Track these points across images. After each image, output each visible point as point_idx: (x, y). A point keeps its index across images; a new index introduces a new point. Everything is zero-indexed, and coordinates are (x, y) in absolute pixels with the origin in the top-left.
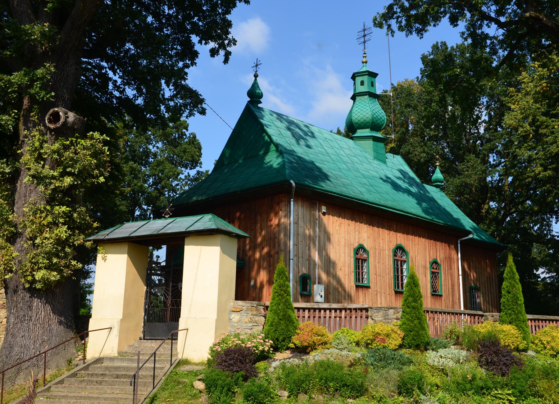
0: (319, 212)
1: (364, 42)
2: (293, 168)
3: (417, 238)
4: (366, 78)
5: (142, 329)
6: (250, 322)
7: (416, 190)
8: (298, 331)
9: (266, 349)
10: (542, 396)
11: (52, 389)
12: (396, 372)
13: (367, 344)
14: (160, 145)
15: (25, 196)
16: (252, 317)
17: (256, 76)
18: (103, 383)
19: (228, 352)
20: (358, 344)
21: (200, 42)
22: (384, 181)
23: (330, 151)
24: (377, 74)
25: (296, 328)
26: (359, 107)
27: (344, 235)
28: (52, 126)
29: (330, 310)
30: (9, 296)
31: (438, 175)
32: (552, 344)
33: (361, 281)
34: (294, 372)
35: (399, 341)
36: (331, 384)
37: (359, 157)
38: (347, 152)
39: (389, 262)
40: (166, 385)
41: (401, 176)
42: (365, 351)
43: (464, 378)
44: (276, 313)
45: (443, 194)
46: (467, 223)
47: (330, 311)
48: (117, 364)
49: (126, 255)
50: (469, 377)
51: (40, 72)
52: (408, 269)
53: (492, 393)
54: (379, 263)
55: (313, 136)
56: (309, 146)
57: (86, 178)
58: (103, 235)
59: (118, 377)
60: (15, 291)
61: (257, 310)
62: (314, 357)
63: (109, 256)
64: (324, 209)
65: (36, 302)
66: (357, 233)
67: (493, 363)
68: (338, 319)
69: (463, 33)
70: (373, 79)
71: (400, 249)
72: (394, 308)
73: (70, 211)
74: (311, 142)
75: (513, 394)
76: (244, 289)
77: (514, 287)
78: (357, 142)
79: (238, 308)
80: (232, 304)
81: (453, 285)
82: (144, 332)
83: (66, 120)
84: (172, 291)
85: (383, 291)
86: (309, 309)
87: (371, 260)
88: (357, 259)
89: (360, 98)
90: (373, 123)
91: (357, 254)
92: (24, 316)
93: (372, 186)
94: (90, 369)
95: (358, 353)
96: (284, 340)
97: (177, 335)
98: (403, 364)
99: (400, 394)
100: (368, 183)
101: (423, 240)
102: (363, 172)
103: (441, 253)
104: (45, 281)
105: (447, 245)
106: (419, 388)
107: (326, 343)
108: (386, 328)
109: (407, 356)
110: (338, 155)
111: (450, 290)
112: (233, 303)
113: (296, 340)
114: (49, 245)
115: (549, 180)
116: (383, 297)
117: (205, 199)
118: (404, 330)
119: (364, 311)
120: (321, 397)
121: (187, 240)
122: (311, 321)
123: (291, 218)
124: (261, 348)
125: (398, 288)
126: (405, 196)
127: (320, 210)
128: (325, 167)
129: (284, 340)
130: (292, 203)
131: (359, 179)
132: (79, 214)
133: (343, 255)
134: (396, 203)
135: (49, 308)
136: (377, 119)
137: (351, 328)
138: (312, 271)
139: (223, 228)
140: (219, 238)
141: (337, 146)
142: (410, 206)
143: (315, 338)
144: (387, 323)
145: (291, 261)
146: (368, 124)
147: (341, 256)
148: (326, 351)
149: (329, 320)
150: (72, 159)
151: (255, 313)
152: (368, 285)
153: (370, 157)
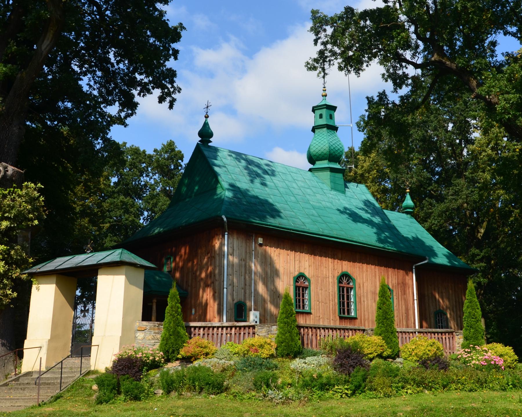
0: (255, 243)
3: (365, 266)
4: (324, 112)
5: (70, 349)
6: (153, 339)
7: (380, 220)
10: (375, 390)
13: (244, 355)
14: (157, 176)
16: (154, 335)
17: (207, 117)
18: (26, 389)
21: (139, 94)
22: (342, 212)
26: (317, 140)
27: (288, 263)
31: (408, 201)
33: (346, 313)
37: (313, 189)
38: (300, 184)
39: (333, 289)
45: (414, 220)
47: (222, 329)
49: (54, 286)
53: (334, 389)
54: (321, 290)
56: (264, 184)
57: (22, 221)
58: (35, 269)
61: (159, 329)
63: (42, 286)
64: (260, 241)
66: (297, 262)
68: (229, 335)
69: (383, 75)
70: (332, 112)
73: (8, 250)
78: (316, 174)
79: (143, 328)
80: (137, 324)
81: (407, 310)
82: (72, 351)
83: (5, 173)
86: (204, 328)
87: (312, 287)
88: (340, 287)
89: (319, 130)
90: (330, 154)
91: (297, 282)
93: (319, 216)
94: (20, 380)
96: (173, 352)
100: (316, 214)
102: (314, 204)
110: (288, 188)
111: (404, 315)
112: (139, 323)
119: (251, 328)
120: (189, 394)
125: (344, 313)
129: (173, 352)
130: (226, 236)
131: (306, 210)
132: (16, 251)
134: (343, 233)
136: (334, 150)
137: (235, 342)
140: (124, 269)
141: (290, 179)
142: (365, 235)
146: (326, 156)
149: (221, 337)
150: (9, 206)
151: (157, 331)
152: (309, 311)
153: (327, 187)
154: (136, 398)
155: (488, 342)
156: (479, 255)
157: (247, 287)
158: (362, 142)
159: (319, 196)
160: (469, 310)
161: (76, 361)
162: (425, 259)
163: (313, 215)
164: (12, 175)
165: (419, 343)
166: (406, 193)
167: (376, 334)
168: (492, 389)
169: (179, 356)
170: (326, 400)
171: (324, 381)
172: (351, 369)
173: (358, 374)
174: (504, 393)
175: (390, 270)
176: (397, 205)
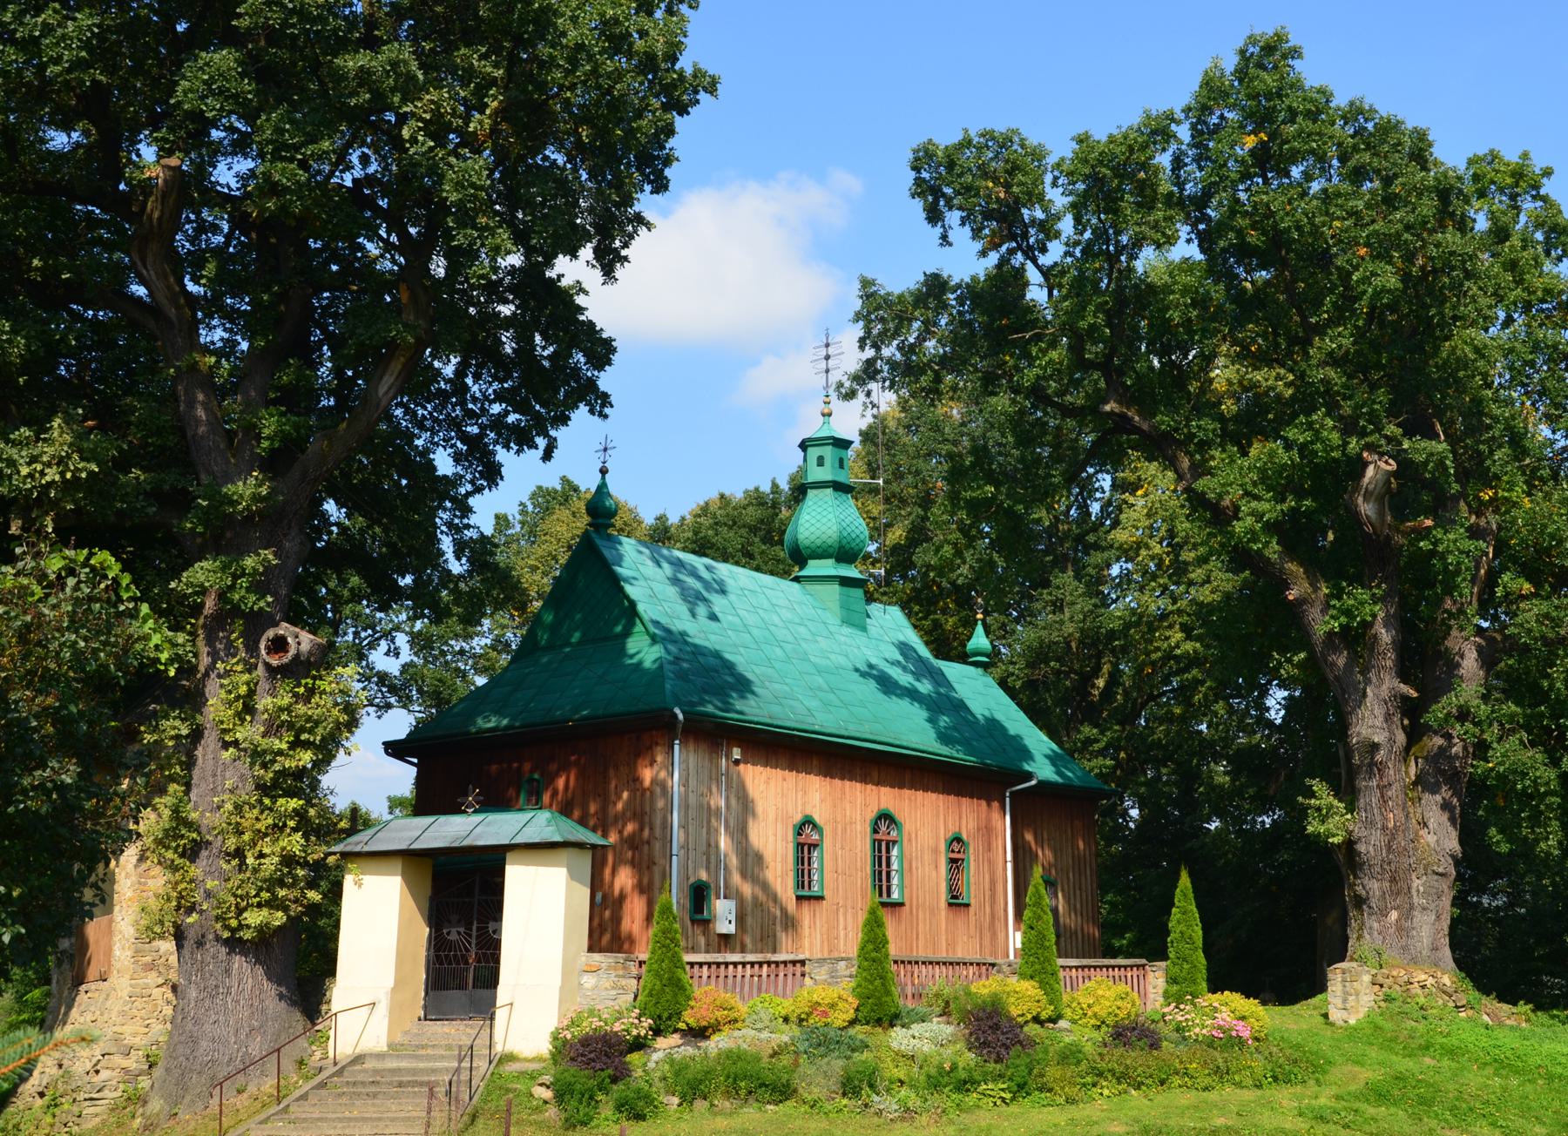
2: (682, 676)
4: (828, 452)
8: (692, 1003)
9: (643, 1033)
10: (1050, 1090)
11: (291, 1109)
12: (841, 1063)
13: (801, 1020)
15: (215, 775)
17: (604, 471)
19: (586, 1041)
20: (786, 1020)
22: (864, 675)
23: (751, 619)
25: (689, 998)
27: (778, 797)
28: (275, 662)
29: (744, 964)
30: (186, 952)
32: (1096, 1009)
34: (687, 1067)
35: (851, 1015)
36: (743, 1084)
40: (489, 1094)
41: (901, 658)
42: (796, 1031)
43: (940, 1067)
44: (658, 975)
46: (1038, 742)
48: (391, 1064)
50: (947, 1066)
51: (249, 562)
52: (901, 857)
55: (723, 592)
56: (713, 617)
59: (400, 1085)
60: (200, 944)
61: (625, 968)
62: (717, 1043)
64: (737, 753)
65: (238, 961)
67: (985, 1044)
70: (842, 453)
71: (885, 818)
72: (847, 959)
74: (718, 603)
75: (1008, 1089)
76: (605, 932)
77: (1039, 918)
81: (993, 883)
82: (425, 1007)
84: (478, 937)
85: (849, 903)
86: (709, 964)
89: (815, 492)
90: (841, 547)
92: (217, 986)
95: (784, 1035)
96: (669, 1018)
97: (493, 1014)
98: (853, 1050)
99: (844, 1094)
101: (932, 797)
104: (262, 929)
105: (984, 803)
106: (871, 1086)
107: (736, 1021)
108: (831, 994)
109: (860, 1037)
111: (988, 893)
113: (689, 1018)
114: (270, 865)
115: (1193, 661)
116: (849, 916)
117: (507, 728)
118: (859, 996)
120: (727, 1104)
121: (509, 856)
122: (712, 987)
123: (674, 772)
124: (635, 1032)
126: (904, 706)
127: (728, 756)
128: (743, 660)
129: (669, 1018)
130: (677, 748)
133: (771, 839)
135: (260, 971)
139: (572, 838)
140: (564, 854)
141: (766, 605)
142: (911, 729)
143: (719, 1014)
144: (831, 989)
147: (772, 839)
148: (736, 1033)
153: (833, 619)
154: (640, 1117)
155: (1215, 988)
156: (1097, 741)
159: (823, 643)
160: (1182, 927)
161: (456, 1032)
163: (820, 689)
164: (310, 652)
165: (1100, 992)
166: (976, 621)
167: (1023, 976)
168: (1239, 1085)
169: (682, 1026)
170: (968, 1110)
171: (963, 1075)
172: (1003, 1051)
173: (1017, 1060)
174: (1259, 1092)
175: (965, 801)
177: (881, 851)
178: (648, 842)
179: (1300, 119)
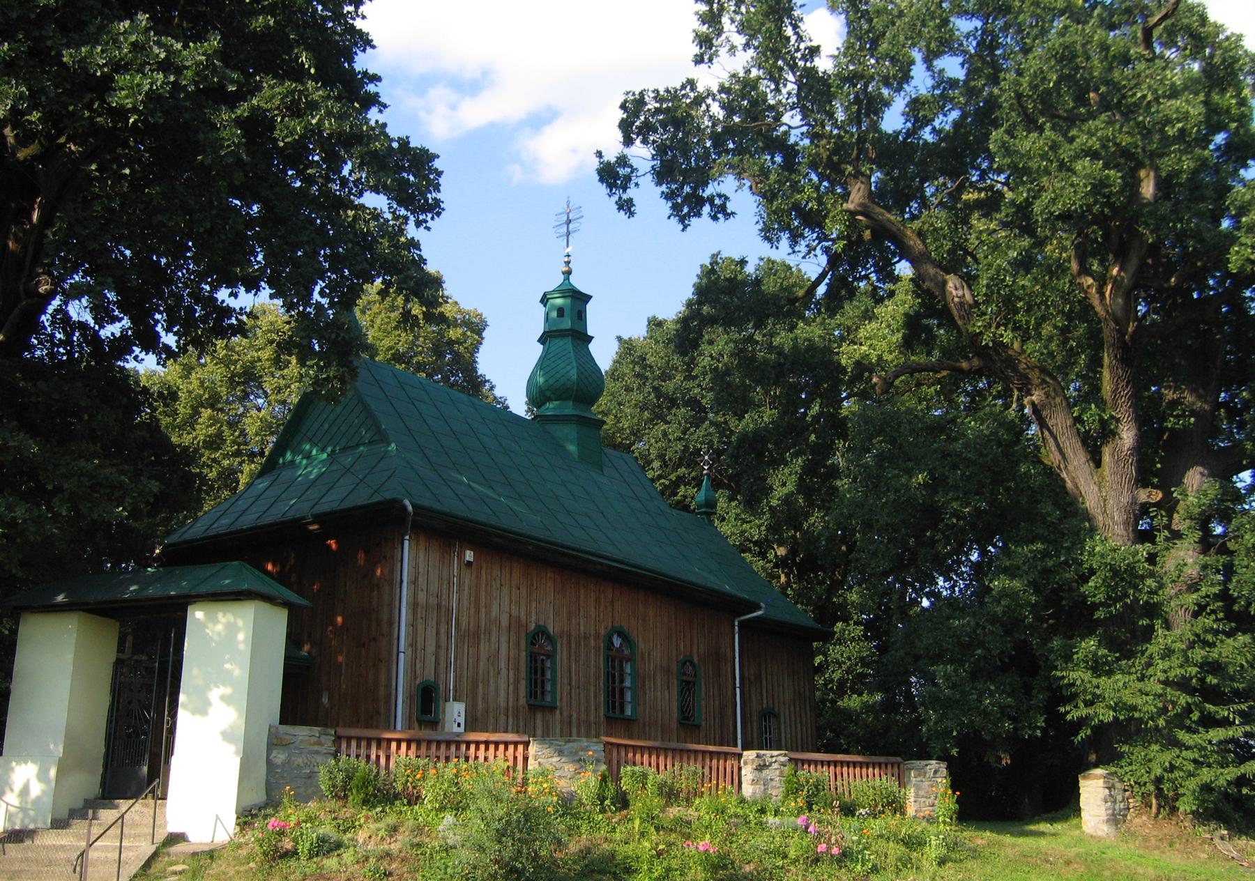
1: (568, 234)
24: (590, 297)
52: (635, 674)
64: (469, 555)
88: (608, 657)
91: (532, 644)
103: (701, 647)
127: (461, 556)
130: (406, 543)
138: (442, 676)
145: (402, 655)
157: (442, 653)
158: (193, 713)
162: (759, 608)
176: (1198, 53)
177: (614, 662)
178: (375, 639)
179: (869, 302)
